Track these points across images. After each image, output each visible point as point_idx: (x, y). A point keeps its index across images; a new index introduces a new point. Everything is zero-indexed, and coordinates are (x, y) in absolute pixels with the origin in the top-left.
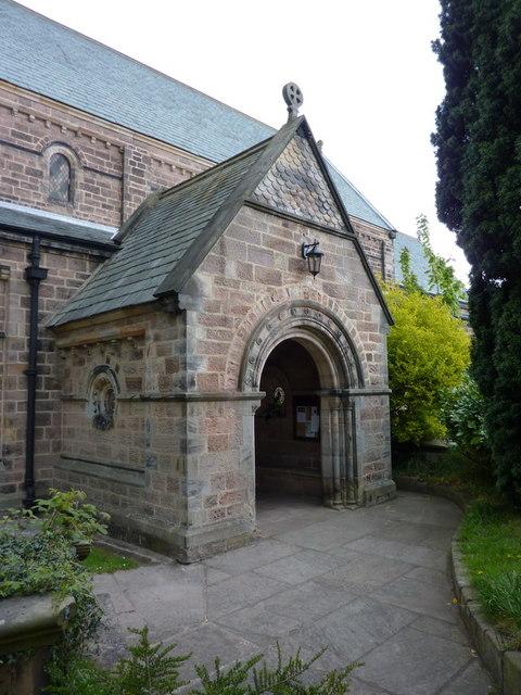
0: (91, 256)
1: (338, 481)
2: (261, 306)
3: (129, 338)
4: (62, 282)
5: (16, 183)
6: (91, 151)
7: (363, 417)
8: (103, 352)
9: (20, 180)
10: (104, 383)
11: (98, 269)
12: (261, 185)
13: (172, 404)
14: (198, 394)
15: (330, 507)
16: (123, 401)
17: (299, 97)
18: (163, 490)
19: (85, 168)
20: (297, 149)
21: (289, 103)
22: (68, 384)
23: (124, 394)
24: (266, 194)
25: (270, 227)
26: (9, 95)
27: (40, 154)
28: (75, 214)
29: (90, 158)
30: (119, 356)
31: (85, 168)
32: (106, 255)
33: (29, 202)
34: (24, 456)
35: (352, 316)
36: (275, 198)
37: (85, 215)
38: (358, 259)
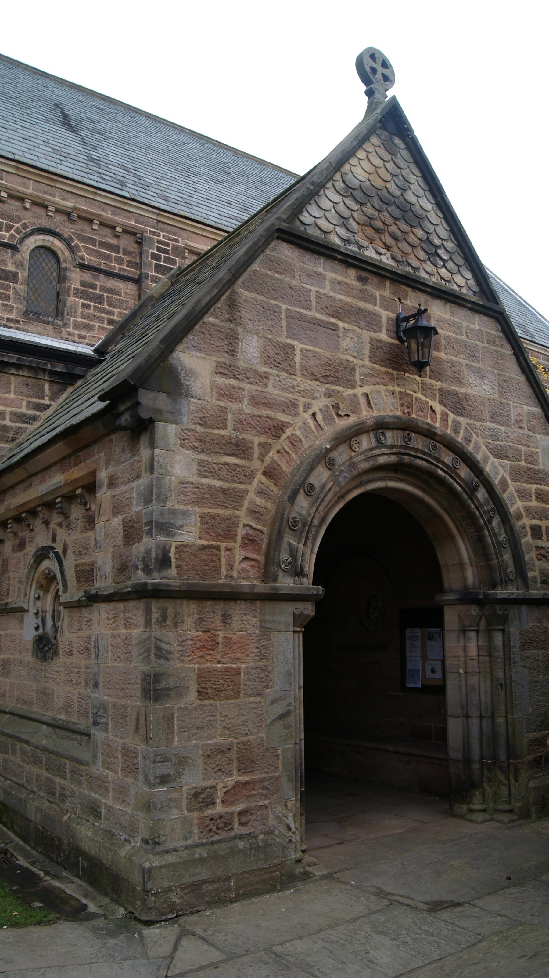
0: (53, 373)
2: (311, 422)
3: (78, 491)
6: (92, 241)
7: (525, 645)
8: (47, 523)
10: (50, 578)
11: (65, 396)
12: (313, 209)
13: (131, 604)
14: (176, 583)
15: (462, 817)
16: (69, 606)
17: (386, 72)
18: (116, 772)
19: (83, 267)
20: (383, 153)
24: (322, 223)
27: (14, 248)
28: (64, 335)
29: (91, 252)
30: (68, 527)
31: (83, 267)
32: (78, 370)
35: (499, 453)
36: (342, 232)
37: (81, 337)
38: (508, 351)
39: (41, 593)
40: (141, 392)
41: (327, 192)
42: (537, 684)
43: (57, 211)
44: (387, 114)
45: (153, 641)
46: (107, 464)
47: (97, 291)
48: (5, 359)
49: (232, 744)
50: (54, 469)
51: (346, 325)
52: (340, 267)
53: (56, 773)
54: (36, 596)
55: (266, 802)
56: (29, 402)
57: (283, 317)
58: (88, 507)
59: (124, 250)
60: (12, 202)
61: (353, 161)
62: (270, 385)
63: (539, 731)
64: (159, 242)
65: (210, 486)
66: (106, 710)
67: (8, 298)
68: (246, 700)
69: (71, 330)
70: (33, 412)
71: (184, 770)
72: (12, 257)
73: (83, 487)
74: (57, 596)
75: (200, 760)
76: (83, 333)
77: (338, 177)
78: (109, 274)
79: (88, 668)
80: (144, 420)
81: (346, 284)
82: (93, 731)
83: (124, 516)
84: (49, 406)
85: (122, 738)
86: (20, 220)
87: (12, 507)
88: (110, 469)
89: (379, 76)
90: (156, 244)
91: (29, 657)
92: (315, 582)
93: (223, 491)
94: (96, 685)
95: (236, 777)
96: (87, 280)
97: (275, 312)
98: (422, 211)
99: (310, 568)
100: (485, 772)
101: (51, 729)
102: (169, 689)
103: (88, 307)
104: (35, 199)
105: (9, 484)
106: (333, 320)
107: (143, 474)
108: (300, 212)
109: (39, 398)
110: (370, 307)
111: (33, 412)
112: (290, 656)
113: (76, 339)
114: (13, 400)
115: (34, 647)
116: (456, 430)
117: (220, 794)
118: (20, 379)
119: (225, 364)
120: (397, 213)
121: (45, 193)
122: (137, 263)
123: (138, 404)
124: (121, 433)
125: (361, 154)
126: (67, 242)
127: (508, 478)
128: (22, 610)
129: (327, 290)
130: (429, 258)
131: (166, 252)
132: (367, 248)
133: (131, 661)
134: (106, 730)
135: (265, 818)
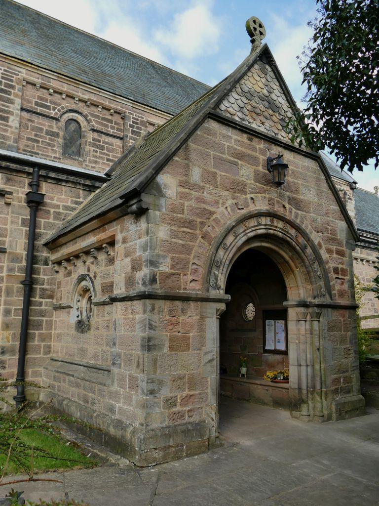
0: (84, 185)
1: (304, 392)
3: (104, 246)
4: (58, 207)
5: (38, 141)
6: (98, 117)
8: (84, 262)
9: (41, 140)
10: (86, 290)
12: (225, 103)
13: (135, 302)
14: (160, 292)
16: (97, 304)
17: (261, 30)
21: (251, 34)
22: (59, 294)
23: (99, 298)
24: (230, 110)
25: (234, 139)
26: (33, 74)
28: (84, 166)
29: (98, 123)
31: (93, 130)
33: (47, 156)
34: (17, 357)
36: (240, 114)
37: (92, 167)
38: (323, 177)
39: (80, 298)
40: (143, 194)
41: (232, 93)
42: (336, 349)
43: (80, 100)
44: (262, 52)
45: (148, 320)
46: (122, 231)
47: (101, 144)
48: (60, 178)
49: (185, 374)
50: (90, 234)
51: (242, 163)
52: (239, 133)
53: (89, 391)
54: (78, 300)
55: (202, 405)
56: (72, 200)
57: (212, 158)
58: (109, 253)
59: (115, 122)
60: (56, 95)
61: (246, 78)
62: (205, 192)
63: (337, 374)
64: (133, 118)
65: (176, 243)
66: (120, 357)
67: (54, 146)
68: (193, 352)
69: (87, 164)
70: (74, 206)
71: (162, 387)
72: (56, 124)
73: (107, 243)
74: (90, 299)
75: (169, 383)
76: (93, 165)
77: (238, 86)
78: (107, 135)
79: (108, 336)
80: (144, 209)
81: (242, 141)
82: (112, 368)
83: (132, 257)
84: (82, 202)
85: (129, 371)
86: (60, 104)
87: (65, 254)
88: (123, 234)
89: (258, 32)
90: (132, 119)
91: (73, 332)
92: (226, 293)
93: (183, 246)
94: (114, 344)
95: (188, 392)
96: (96, 137)
97: (207, 155)
98: (279, 104)
99: (223, 286)
100: (309, 395)
101: (86, 368)
102: (155, 345)
103: (96, 152)
104: (68, 94)
105: (64, 242)
106: (236, 160)
107: (143, 236)
108: (220, 104)
109: (77, 198)
110: (253, 153)
111: (74, 206)
112: (215, 331)
113: (90, 168)
114: (64, 199)
115: (76, 327)
116: (296, 217)
117: (179, 400)
118: (67, 188)
119: (183, 181)
120: (267, 105)
121: (73, 91)
122: (122, 129)
123: (141, 200)
124: (130, 215)
125: (250, 74)
126: (85, 117)
127: (322, 242)
128: (70, 307)
129: (233, 144)
130: (283, 129)
131: (137, 123)
132: (252, 123)
133: (135, 331)
134: (120, 367)
135: (201, 414)
